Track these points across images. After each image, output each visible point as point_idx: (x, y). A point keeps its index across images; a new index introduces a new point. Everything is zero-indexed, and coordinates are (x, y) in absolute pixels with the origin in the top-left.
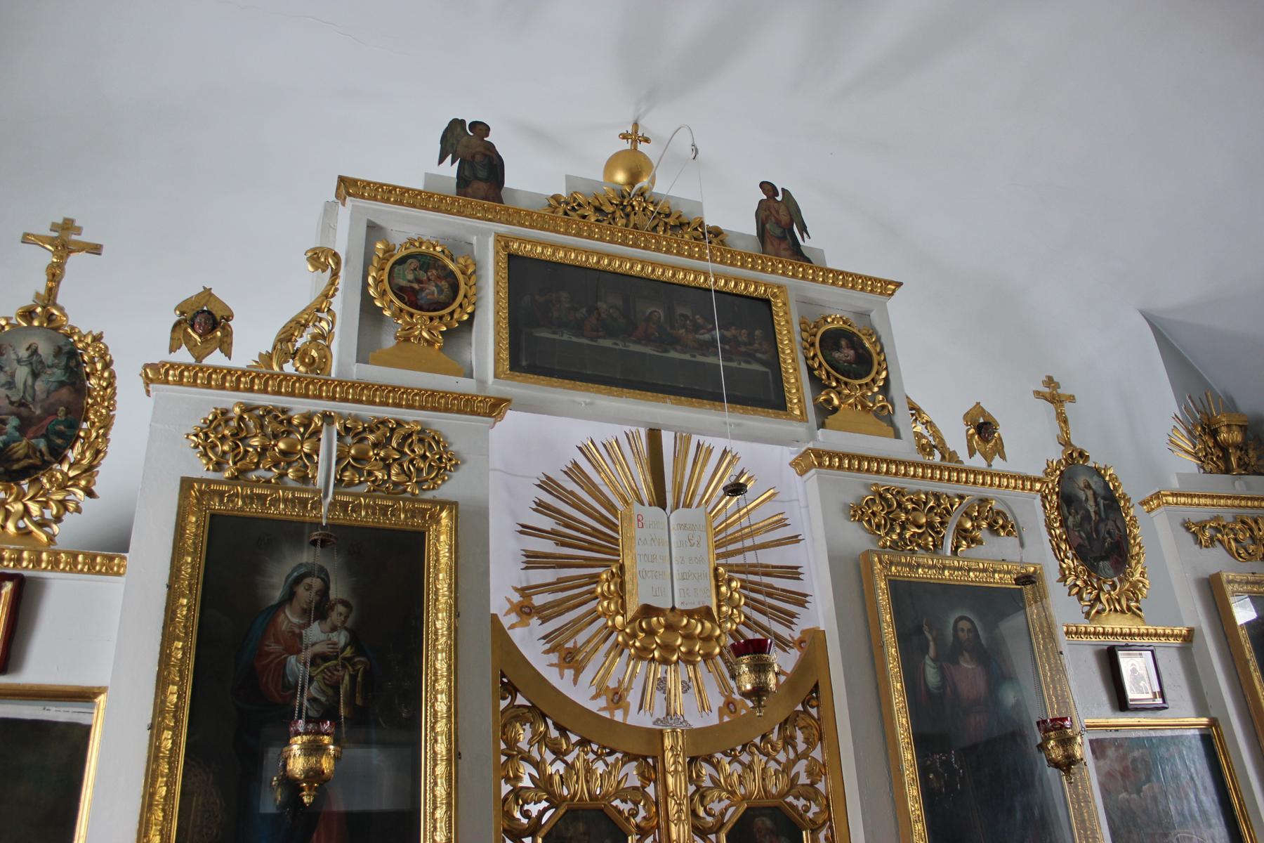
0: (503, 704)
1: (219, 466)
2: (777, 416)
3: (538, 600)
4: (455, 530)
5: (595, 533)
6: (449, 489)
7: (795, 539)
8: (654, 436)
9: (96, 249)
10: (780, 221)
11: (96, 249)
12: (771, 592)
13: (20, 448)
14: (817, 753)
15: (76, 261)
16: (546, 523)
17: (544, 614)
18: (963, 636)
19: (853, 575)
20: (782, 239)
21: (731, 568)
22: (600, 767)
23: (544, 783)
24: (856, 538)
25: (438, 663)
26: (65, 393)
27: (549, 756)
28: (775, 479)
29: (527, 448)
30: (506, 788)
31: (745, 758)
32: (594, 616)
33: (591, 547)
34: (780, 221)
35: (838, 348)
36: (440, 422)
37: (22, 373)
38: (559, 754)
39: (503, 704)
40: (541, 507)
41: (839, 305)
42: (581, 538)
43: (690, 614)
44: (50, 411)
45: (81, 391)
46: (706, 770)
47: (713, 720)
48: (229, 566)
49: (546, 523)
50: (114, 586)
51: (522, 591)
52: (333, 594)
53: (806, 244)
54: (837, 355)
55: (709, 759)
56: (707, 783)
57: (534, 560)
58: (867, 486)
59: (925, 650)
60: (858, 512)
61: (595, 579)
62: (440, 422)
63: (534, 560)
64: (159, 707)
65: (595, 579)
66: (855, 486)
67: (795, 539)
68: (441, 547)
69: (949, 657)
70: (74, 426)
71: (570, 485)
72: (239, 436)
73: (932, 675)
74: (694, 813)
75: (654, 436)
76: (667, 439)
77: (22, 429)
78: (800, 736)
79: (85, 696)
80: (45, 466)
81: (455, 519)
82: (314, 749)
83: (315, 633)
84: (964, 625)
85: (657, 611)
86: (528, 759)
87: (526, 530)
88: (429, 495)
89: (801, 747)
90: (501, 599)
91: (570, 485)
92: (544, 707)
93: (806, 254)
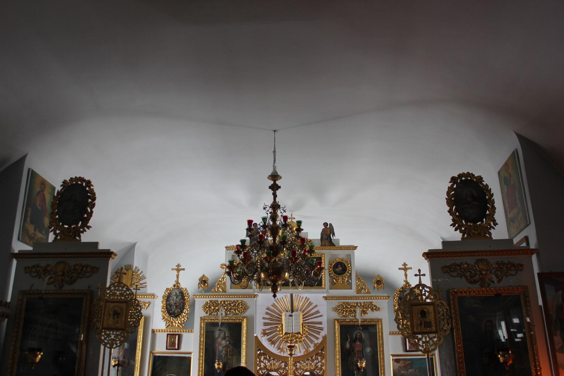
0: (258, 352)
1: (207, 313)
2: (319, 288)
3: (267, 332)
4: (247, 322)
5: (278, 317)
6: (247, 313)
7: (321, 316)
8: (292, 295)
9: (184, 269)
10: (328, 232)
11: (184, 269)
12: (315, 327)
13: (176, 311)
14: (323, 361)
15: (181, 272)
16: (268, 316)
17: (267, 334)
18: (358, 337)
19: (332, 323)
20: (327, 239)
21: (306, 323)
22: (277, 364)
23: (265, 367)
24: (335, 315)
25: (244, 346)
26: (182, 300)
27: (267, 362)
28: (319, 302)
29: (261, 302)
30: (258, 368)
31: (307, 362)
32: (277, 335)
33: (277, 320)
34: (328, 232)
35: (337, 267)
36: (245, 300)
37: (175, 297)
38: (269, 361)
39: (258, 352)
40: (267, 313)
41: (341, 255)
42: (274, 319)
43: (296, 333)
44: (180, 304)
45: (184, 299)
46: (298, 364)
47: (302, 354)
48: (209, 332)
49: (268, 316)
50: (192, 334)
51: (263, 330)
52: (226, 335)
53: (333, 238)
54: (337, 270)
55: (299, 362)
56: (298, 367)
57: (265, 324)
58: (339, 303)
59: (347, 340)
60: (336, 309)
61: (277, 327)
62: (245, 300)
63: (265, 324)
64: (200, 349)
65: (277, 327)
66: (336, 303)
67: (321, 316)
68: (244, 324)
69: (353, 341)
70: (184, 306)
71: (272, 308)
72: (210, 307)
73: (348, 346)
74: (295, 373)
75: (292, 295)
76: (294, 295)
77: (176, 308)
78: (319, 358)
79: (190, 353)
80: (180, 314)
81: (247, 320)
82: (219, 364)
83: (224, 342)
84: (358, 334)
85: (289, 334)
86: (263, 362)
87: (264, 318)
88: (243, 315)
89: (320, 360)
90: (258, 333)
91: (272, 308)
92: (266, 353)
93: (333, 242)
